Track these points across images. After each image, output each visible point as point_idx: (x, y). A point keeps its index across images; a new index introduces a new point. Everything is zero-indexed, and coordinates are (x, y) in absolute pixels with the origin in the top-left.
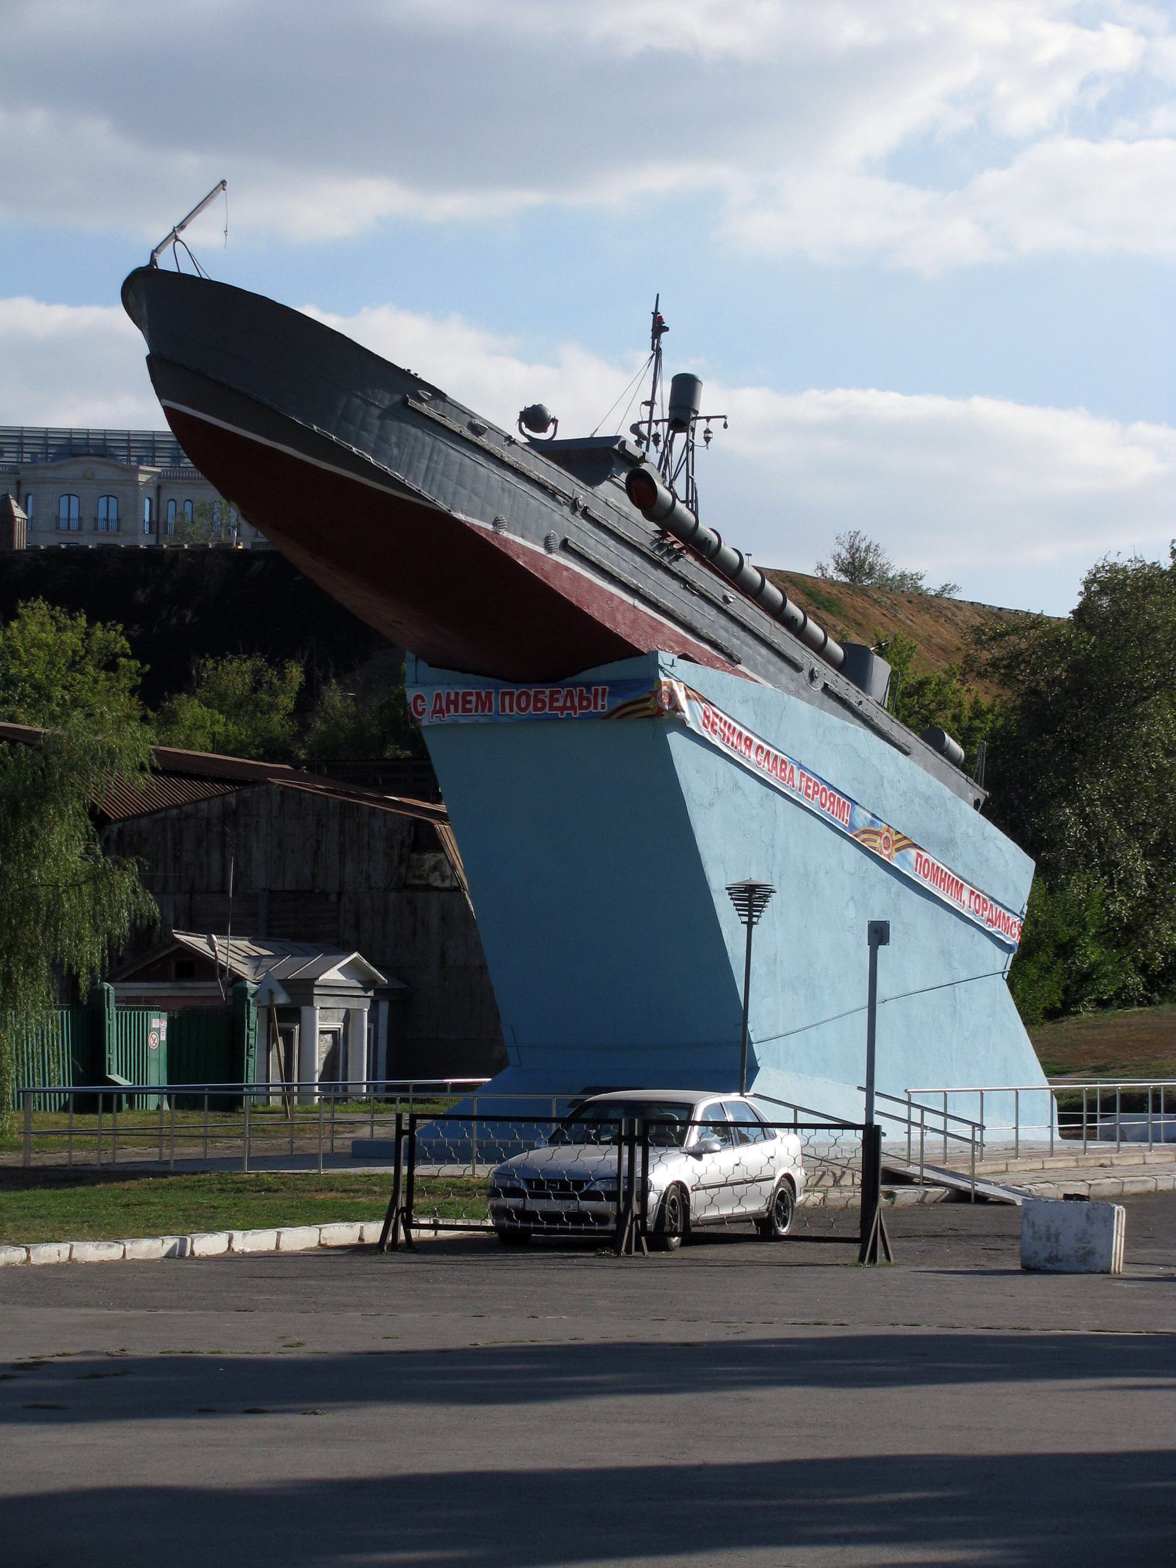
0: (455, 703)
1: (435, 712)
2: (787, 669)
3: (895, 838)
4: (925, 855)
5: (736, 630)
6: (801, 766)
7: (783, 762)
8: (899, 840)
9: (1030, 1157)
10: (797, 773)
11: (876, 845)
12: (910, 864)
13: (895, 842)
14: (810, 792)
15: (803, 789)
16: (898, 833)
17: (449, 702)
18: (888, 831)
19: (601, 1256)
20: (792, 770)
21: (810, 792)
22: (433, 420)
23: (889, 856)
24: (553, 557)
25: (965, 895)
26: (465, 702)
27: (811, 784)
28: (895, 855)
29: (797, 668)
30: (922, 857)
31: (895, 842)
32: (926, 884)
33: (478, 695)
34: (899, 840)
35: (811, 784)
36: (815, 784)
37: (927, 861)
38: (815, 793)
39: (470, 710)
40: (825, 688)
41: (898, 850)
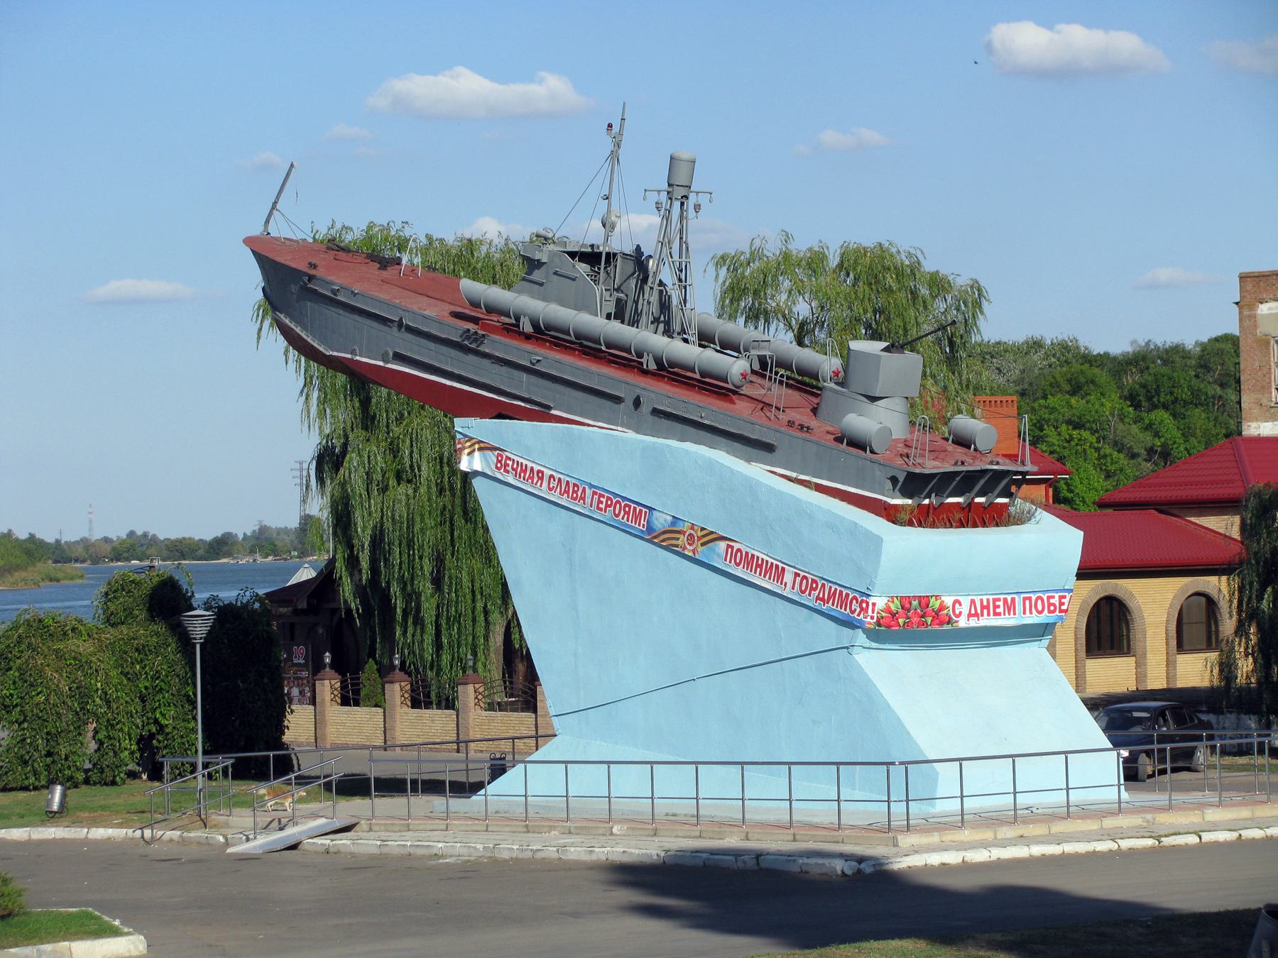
0: (988, 607)
1: (970, 615)
2: (607, 404)
3: (700, 534)
4: (736, 546)
5: (505, 370)
6: (591, 486)
7: (575, 485)
8: (704, 536)
9: (1083, 818)
10: (589, 492)
11: (679, 542)
12: (718, 555)
13: (699, 539)
14: (602, 506)
15: (595, 503)
16: (703, 529)
17: (983, 607)
18: (692, 528)
19: (846, 857)
20: (584, 490)
21: (602, 506)
22: (587, 347)
23: (694, 551)
24: (389, 366)
25: (788, 577)
26: (996, 607)
27: (604, 500)
28: (700, 549)
29: (617, 400)
30: (732, 547)
31: (699, 539)
32: (739, 572)
33: (1005, 600)
34: (704, 536)
35: (604, 500)
36: (608, 498)
37: (739, 550)
38: (607, 506)
39: (999, 614)
40: (656, 412)
41: (703, 545)
